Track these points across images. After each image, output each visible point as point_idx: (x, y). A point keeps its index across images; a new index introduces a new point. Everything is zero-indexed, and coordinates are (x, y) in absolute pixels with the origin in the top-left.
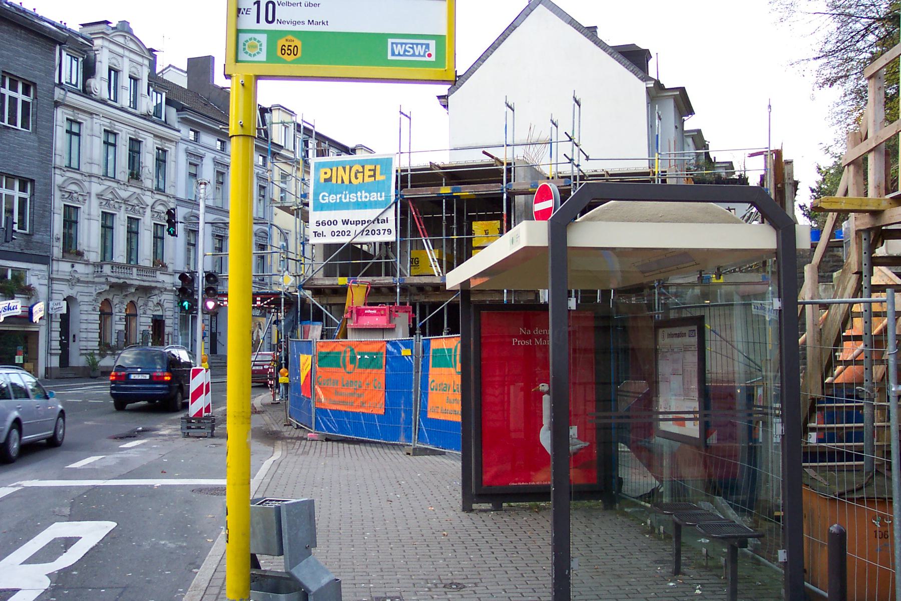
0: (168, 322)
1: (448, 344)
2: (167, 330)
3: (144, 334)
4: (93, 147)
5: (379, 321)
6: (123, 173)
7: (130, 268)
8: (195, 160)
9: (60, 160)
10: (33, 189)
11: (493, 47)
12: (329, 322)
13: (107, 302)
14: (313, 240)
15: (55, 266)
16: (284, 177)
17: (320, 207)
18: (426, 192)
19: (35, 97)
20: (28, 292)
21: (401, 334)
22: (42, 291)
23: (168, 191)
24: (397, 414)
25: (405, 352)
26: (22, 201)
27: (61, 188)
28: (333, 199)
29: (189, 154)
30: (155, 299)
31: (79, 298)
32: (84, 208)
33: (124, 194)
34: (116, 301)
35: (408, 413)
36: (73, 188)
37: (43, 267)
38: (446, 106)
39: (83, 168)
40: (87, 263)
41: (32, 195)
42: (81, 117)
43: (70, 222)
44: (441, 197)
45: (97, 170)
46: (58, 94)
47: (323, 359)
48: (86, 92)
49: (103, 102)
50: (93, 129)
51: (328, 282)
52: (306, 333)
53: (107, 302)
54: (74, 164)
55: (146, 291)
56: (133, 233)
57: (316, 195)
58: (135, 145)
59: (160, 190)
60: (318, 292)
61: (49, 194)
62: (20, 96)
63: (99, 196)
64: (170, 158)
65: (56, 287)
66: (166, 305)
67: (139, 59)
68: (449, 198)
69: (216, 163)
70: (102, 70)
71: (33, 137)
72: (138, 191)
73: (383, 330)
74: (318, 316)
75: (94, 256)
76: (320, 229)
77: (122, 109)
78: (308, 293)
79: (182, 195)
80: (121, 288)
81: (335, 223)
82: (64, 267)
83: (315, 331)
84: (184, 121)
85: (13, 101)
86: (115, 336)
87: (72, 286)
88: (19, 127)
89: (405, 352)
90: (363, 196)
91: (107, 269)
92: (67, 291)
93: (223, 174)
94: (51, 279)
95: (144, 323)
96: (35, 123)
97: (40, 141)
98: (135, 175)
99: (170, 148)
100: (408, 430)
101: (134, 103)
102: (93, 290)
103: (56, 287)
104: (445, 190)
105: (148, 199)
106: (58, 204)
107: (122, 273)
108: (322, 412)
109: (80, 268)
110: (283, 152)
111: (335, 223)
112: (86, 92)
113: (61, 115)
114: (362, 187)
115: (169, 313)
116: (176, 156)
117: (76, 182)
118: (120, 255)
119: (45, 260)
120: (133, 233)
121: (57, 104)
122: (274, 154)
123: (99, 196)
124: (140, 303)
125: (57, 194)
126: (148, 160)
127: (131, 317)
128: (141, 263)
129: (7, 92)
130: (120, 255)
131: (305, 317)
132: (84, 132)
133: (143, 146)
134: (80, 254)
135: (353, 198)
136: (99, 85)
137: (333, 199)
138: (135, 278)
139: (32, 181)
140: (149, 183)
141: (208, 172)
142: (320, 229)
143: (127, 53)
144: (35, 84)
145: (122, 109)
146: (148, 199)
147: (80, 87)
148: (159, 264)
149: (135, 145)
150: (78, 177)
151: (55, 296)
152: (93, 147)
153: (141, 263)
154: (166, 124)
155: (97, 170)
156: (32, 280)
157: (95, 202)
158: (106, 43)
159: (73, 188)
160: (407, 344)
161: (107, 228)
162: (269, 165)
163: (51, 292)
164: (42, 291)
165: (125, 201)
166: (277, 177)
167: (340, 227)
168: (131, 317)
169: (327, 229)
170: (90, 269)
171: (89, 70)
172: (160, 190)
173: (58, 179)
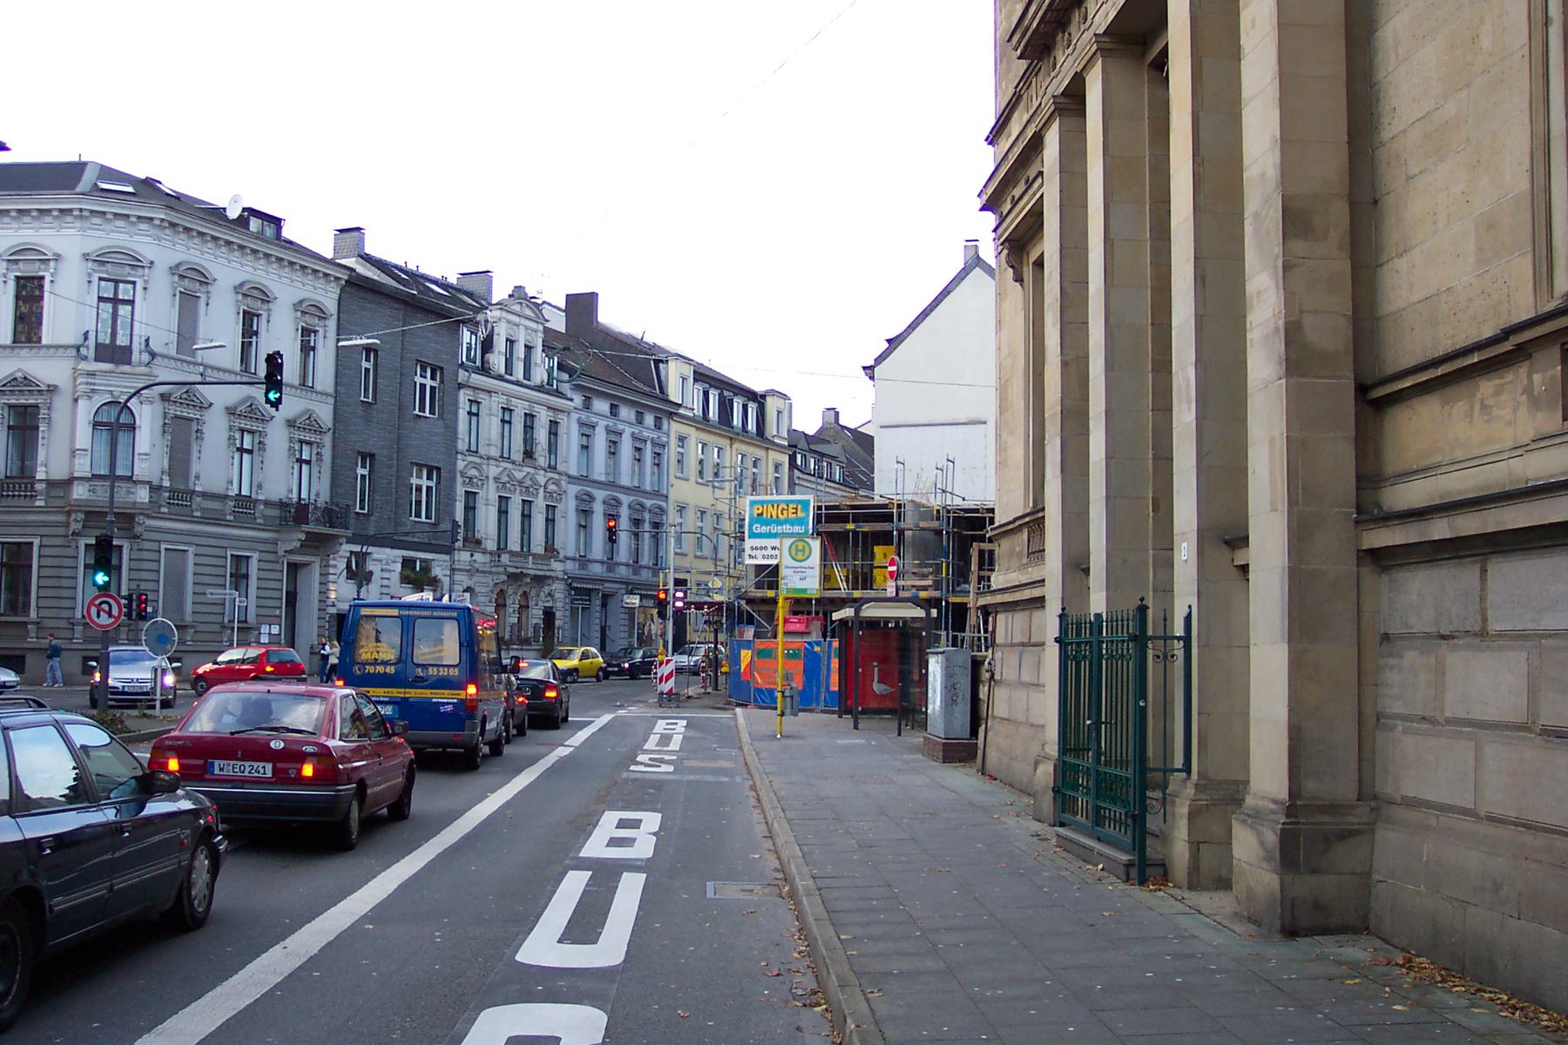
0: (558, 614)
1: (149, 676)
2: (557, 623)
3: (536, 626)
4: (491, 426)
5: (799, 627)
6: (518, 456)
7: (526, 557)
8: (587, 429)
9: (462, 446)
10: (439, 477)
11: (925, 314)
12: (759, 625)
13: (502, 593)
14: (748, 561)
15: (457, 555)
16: (682, 439)
17: (753, 535)
18: (836, 527)
19: (442, 381)
20: (434, 583)
21: (815, 636)
22: (446, 581)
23: (559, 467)
24: (811, 688)
25: (817, 649)
26: (429, 489)
27: (463, 474)
28: (764, 529)
29: (582, 424)
30: (546, 589)
31: (477, 589)
32: (482, 493)
33: (519, 475)
34: (510, 591)
35: (818, 688)
36: (473, 472)
37: (447, 557)
38: (872, 378)
39: (482, 451)
40: (485, 552)
41: (438, 483)
42: (482, 396)
43: (470, 509)
44: (847, 532)
45: (495, 452)
46: (462, 375)
47: (759, 653)
48: (485, 370)
49: (500, 378)
50: (491, 407)
51: (759, 594)
52: (742, 634)
53: (502, 593)
54: (473, 448)
55: (540, 580)
56: (526, 517)
57: (751, 526)
58: (529, 417)
59: (553, 468)
60: (750, 601)
61: (454, 480)
62: (429, 382)
63: (496, 479)
64: (562, 431)
65: (457, 577)
66: (557, 595)
67: (534, 325)
68: (854, 532)
69: (609, 431)
70: (500, 344)
71: (440, 423)
72: (532, 471)
73: (802, 634)
74: (751, 621)
75: (491, 545)
76: (754, 553)
77: (517, 383)
78: (743, 603)
79: (573, 472)
80: (514, 578)
81: (765, 548)
82: (464, 556)
83: (749, 633)
84: (578, 388)
85: (423, 386)
86: (508, 629)
87: (471, 577)
88: (427, 414)
89: (817, 649)
90: (787, 528)
91: (505, 558)
92: (467, 583)
93: (615, 443)
94: (453, 570)
95: (536, 615)
96: (441, 407)
97: (446, 427)
98: (529, 454)
99: (562, 418)
100: (818, 699)
101: (527, 375)
102: (489, 580)
103: (457, 577)
104: (850, 526)
105: (541, 478)
106: (460, 490)
107: (519, 561)
108: (759, 690)
109: (478, 557)
110: (681, 411)
111: (765, 548)
112: (485, 370)
113: (464, 396)
114: (786, 521)
115: (559, 605)
116: (568, 428)
117: (477, 467)
118: (514, 544)
119: (448, 550)
120: (526, 517)
121: (460, 386)
122: (671, 415)
123: (496, 479)
124: (533, 593)
125: (459, 480)
126: (541, 435)
127: (524, 608)
128: (534, 550)
129: (418, 380)
130: (514, 544)
131: (740, 622)
132: (483, 412)
133: (536, 420)
134: (478, 542)
135: (779, 529)
136: (497, 361)
137: (764, 529)
138: (531, 568)
139: (438, 469)
140: (542, 461)
141: (600, 441)
142: (754, 553)
143: (523, 321)
144: (442, 369)
145: (517, 383)
146: (541, 478)
147: (478, 363)
148: (551, 550)
149: (529, 417)
150: (477, 460)
151: (456, 587)
152: (491, 426)
153: (534, 550)
154: (558, 393)
155: (495, 452)
156: (438, 571)
157: (492, 485)
158: (504, 314)
159: (473, 472)
160: (818, 644)
161: (503, 513)
162: (665, 426)
163: (452, 583)
164: (446, 581)
165: (520, 482)
166: (673, 442)
167: (770, 552)
168: (524, 608)
169: (759, 553)
170: (487, 558)
171: (487, 345)
172: (553, 468)
173: (460, 464)
